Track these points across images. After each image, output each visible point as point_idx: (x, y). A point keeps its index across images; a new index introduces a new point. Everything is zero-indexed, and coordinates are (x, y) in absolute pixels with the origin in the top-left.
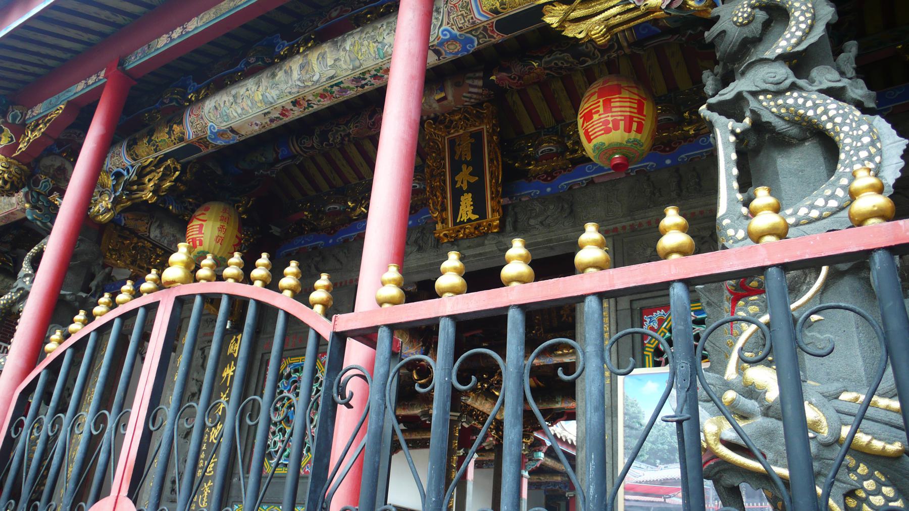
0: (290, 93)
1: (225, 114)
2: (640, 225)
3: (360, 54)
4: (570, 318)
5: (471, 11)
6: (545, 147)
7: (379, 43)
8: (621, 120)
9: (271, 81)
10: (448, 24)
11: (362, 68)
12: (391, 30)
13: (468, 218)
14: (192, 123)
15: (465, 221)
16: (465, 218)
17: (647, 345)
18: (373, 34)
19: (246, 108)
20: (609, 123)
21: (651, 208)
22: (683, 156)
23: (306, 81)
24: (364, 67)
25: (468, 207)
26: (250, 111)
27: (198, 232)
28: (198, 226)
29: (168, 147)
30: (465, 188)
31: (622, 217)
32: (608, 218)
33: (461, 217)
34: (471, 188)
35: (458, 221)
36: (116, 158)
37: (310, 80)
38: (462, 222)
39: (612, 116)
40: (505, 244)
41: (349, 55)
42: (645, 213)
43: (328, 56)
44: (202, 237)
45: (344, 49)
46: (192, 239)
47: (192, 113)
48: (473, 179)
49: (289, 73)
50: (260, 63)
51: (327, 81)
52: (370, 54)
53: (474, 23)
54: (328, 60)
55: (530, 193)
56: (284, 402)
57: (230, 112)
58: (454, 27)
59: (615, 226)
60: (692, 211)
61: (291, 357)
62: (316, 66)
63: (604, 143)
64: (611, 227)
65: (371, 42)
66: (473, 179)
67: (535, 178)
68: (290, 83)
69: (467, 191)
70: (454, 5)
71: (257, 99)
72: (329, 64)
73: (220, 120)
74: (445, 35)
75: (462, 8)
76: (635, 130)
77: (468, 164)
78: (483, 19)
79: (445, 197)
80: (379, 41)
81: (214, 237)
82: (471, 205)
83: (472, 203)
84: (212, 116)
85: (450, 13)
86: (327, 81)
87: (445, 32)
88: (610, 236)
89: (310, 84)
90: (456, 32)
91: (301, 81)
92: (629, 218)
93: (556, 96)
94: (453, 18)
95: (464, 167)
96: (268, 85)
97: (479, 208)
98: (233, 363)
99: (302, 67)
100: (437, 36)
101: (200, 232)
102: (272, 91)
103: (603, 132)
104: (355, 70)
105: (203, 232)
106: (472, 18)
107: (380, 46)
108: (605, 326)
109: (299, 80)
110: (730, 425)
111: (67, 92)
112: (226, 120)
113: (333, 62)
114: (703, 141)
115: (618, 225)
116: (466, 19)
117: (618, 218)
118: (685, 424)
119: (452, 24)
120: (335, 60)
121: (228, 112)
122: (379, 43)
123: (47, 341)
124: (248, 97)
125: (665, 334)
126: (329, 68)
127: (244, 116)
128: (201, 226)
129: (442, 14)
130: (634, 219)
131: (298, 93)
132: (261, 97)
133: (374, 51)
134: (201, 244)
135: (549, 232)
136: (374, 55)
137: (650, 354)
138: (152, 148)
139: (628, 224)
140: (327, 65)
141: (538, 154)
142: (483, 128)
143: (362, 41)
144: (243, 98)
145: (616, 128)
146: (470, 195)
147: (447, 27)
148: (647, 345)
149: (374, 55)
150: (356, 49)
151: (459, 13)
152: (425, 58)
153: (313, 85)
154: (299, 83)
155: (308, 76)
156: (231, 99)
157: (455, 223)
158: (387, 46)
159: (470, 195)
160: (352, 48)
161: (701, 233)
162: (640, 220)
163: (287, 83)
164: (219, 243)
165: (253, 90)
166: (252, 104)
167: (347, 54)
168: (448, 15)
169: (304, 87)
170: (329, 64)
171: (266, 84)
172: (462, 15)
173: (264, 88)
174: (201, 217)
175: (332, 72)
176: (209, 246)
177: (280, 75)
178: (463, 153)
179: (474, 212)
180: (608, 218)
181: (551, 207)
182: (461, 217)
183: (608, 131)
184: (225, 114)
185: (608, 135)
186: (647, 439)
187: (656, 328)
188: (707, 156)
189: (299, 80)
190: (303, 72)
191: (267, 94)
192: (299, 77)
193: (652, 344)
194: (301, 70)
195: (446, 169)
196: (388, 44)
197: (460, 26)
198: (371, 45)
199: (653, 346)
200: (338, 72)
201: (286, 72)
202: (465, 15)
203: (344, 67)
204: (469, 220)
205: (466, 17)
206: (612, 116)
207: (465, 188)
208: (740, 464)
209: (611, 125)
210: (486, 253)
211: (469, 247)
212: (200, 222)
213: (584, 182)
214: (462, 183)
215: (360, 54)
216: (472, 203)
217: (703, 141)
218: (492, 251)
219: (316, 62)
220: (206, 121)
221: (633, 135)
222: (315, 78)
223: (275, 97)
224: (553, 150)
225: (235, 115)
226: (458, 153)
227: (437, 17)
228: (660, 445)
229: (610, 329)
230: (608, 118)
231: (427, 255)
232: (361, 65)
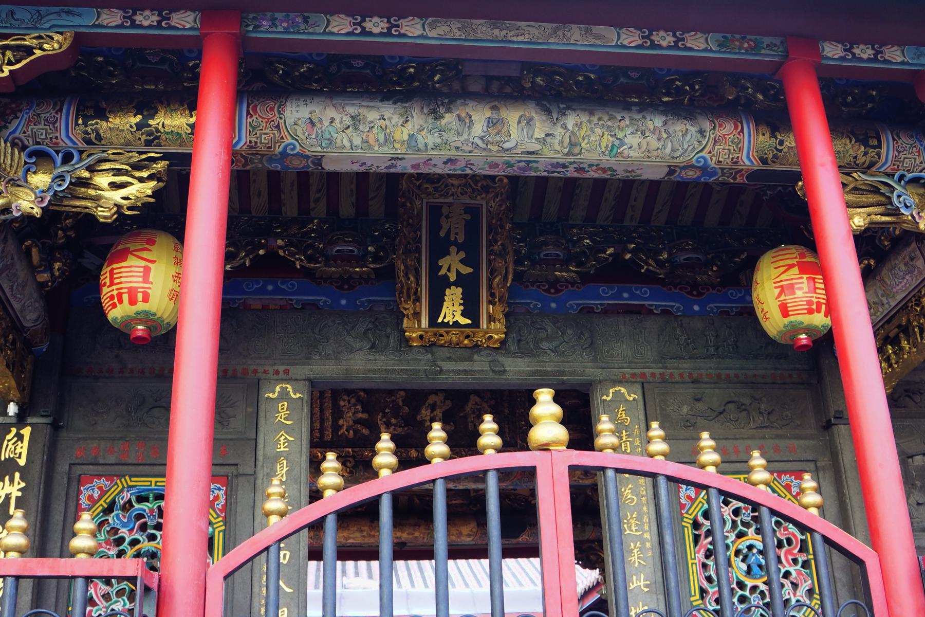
0: (457, 148)
1: (327, 136)
2: (671, 375)
3: (586, 141)
4: (351, 432)
5: (741, 150)
6: (551, 250)
7: (617, 138)
8: (824, 304)
9: (430, 121)
10: (710, 152)
11: (579, 157)
12: (637, 130)
13: (455, 320)
14: (254, 128)
15: (451, 323)
16: (449, 319)
17: (685, 515)
18: (609, 123)
19: (371, 141)
20: (813, 304)
21: (686, 359)
22: (712, 305)
23: (492, 143)
24: (582, 157)
25: (457, 305)
26: (376, 148)
27: (141, 279)
28: (142, 269)
29: (180, 146)
30: (453, 277)
31: (651, 363)
32: (636, 360)
33: (445, 317)
34: (461, 281)
35: (440, 320)
36: (42, 126)
37: (498, 143)
38: (445, 325)
39: (817, 298)
40: (503, 366)
41: (570, 137)
42: (679, 363)
43: (537, 125)
44: (149, 288)
45: (564, 127)
46: (129, 288)
47: (255, 112)
48: (466, 270)
49: (466, 122)
50: (368, 71)
51: (522, 154)
52: (600, 147)
53: (736, 163)
54: (536, 130)
55: (529, 304)
56: (121, 548)
57: (340, 138)
58: (714, 158)
59: (642, 371)
60: (727, 372)
61: (131, 476)
62: (515, 131)
63: (803, 323)
64: (638, 371)
65: (606, 133)
66: (466, 270)
67: (533, 284)
68: (465, 136)
69: (456, 284)
70: (724, 135)
71: (397, 136)
72: (536, 136)
73: (314, 142)
74: (700, 162)
75: (732, 143)
77: (460, 248)
78: (747, 163)
79: (418, 284)
80: (618, 136)
81: (167, 291)
82: (460, 304)
83: (462, 302)
84: (299, 133)
85: (717, 142)
86: (522, 154)
87: (701, 159)
88: (639, 382)
89: (495, 148)
90: (712, 164)
91: (483, 141)
92: (661, 365)
93: (577, 191)
94: (718, 149)
95: (453, 249)
96: (425, 126)
97: (471, 308)
98: (7, 478)
99: (491, 123)
100: (691, 159)
101: (146, 279)
102: (430, 136)
103: (806, 311)
104: (569, 155)
105: (151, 280)
106: (738, 157)
107: (617, 143)
108: (642, 489)
109: (481, 138)
111: (69, 13)
112: (323, 145)
113: (543, 136)
114: (732, 294)
115: (647, 372)
116: (731, 156)
117: (648, 362)
119: (714, 154)
120: (547, 135)
121: (335, 135)
122: (617, 138)
124: (383, 129)
125: (703, 504)
126: (534, 141)
127: (359, 151)
128: (147, 270)
129: (707, 139)
130: (666, 368)
131: (470, 152)
132: (406, 137)
133: (607, 146)
134: (146, 299)
135: (564, 362)
136: (604, 149)
137: (689, 526)
138: (144, 137)
139: (657, 371)
140: (532, 136)
141: (539, 255)
142: (482, 205)
143: (593, 126)
144: (373, 127)
145: (819, 311)
146: (460, 290)
147: (708, 156)
148: (685, 515)
149: (604, 149)
150: (583, 133)
151: (727, 147)
152: (359, 57)
153: (498, 151)
154: (480, 142)
155: (498, 139)
156: (348, 121)
157: (433, 322)
158: (625, 147)
159: (460, 290)
160: (577, 129)
161: (741, 400)
162: (672, 370)
163: (459, 134)
164: (173, 301)
165: (394, 121)
166: (386, 140)
167: (568, 134)
168: (714, 144)
169: (484, 149)
170: (536, 136)
171: (421, 122)
172: (729, 150)
173: (417, 127)
174: (144, 254)
175: (536, 147)
176: (165, 310)
177: (449, 119)
178: (453, 231)
179: (464, 314)
180: (636, 360)
181: (570, 332)
182: (445, 317)
183: (810, 312)
184: (327, 136)
185: (810, 315)
187: (693, 497)
188: (736, 312)
189: (481, 138)
190: (492, 131)
191: (419, 137)
192: (483, 134)
193: (690, 515)
194: (488, 127)
195: (421, 244)
196: (629, 146)
197: (720, 160)
198: (606, 136)
199: (692, 517)
200: (545, 150)
202: (732, 151)
203: (557, 147)
204: (456, 324)
205: (733, 154)
206: (817, 298)
207: (453, 277)
209: (814, 307)
210: (474, 371)
211: (449, 359)
212: (144, 263)
213: (599, 306)
214: (449, 270)
215: (586, 141)
216: (462, 302)
217: (732, 294)
218: (483, 371)
219: (516, 126)
220: (284, 133)
222: (507, 145)
223: (430, 145)
224: (560, 256)
225: (347, 144)
226: (445, 227)
227: (700, 139)
229: (646, 493)
230: (813, 299)
231: (382, 358)
232: (580, 153)
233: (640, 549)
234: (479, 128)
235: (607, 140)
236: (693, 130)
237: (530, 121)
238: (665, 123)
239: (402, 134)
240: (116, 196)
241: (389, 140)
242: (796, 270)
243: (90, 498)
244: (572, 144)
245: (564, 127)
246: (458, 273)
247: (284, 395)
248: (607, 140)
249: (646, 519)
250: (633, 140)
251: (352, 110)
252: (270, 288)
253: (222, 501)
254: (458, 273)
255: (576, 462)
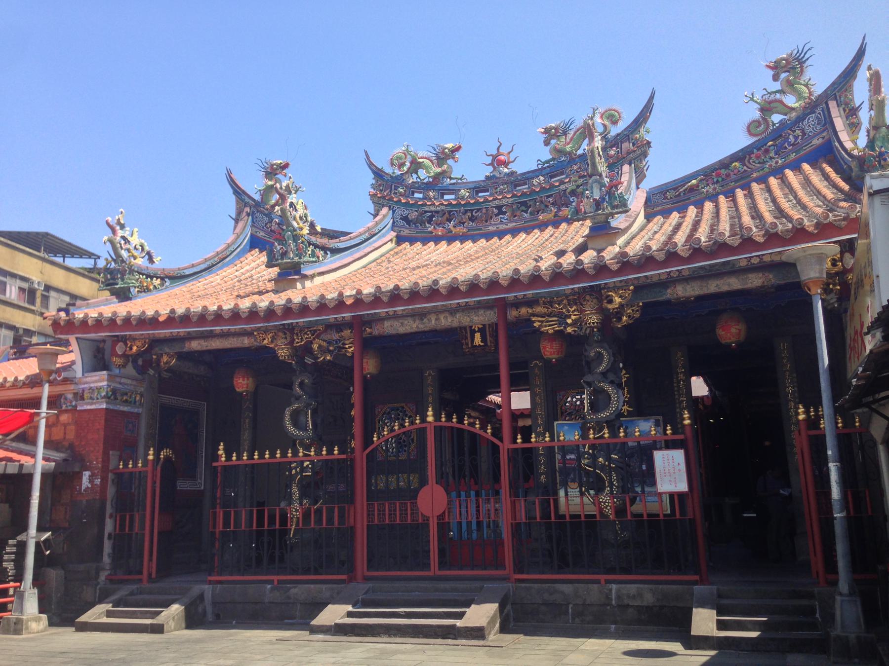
16: (477, 344)
30: (477, 329)
38: (476, 346)
45: (456, 318)
49: (430, 320)
69: (478, 332)
76: (476, 529)
79: (466, 333)
99: (436, 319)
110: (883, 419)
118: (68, 427)
123: (667, 430)
145: (554, 354)
175: (450, 324)
177: (425, 320)
183: (551, 355)
186: (45, 264)
201: (428, 320)
207: (477, 329)
208: (840, 486)
221: (559, 356)
228: (178, 292)
233: (541, 418)
234: (433, 322)
235: (468, 319)
236: (492, 312)
237: (447, 317)
238: (484, 312)
239: (415, 326)
240: (350, 350)
241: (412, 328)
242: (547, 341)
243: (378, 411)
244: (459, 322)
245: (456, 318)
246: (478, 327)
247: (430, 374)
248: (468, 319)
249: (543, 408)
250: (476, 318)
251: (401, 321)
252: (424, 337)
253: (415, 409)
254: (478, 327)
255: (428, 429)
